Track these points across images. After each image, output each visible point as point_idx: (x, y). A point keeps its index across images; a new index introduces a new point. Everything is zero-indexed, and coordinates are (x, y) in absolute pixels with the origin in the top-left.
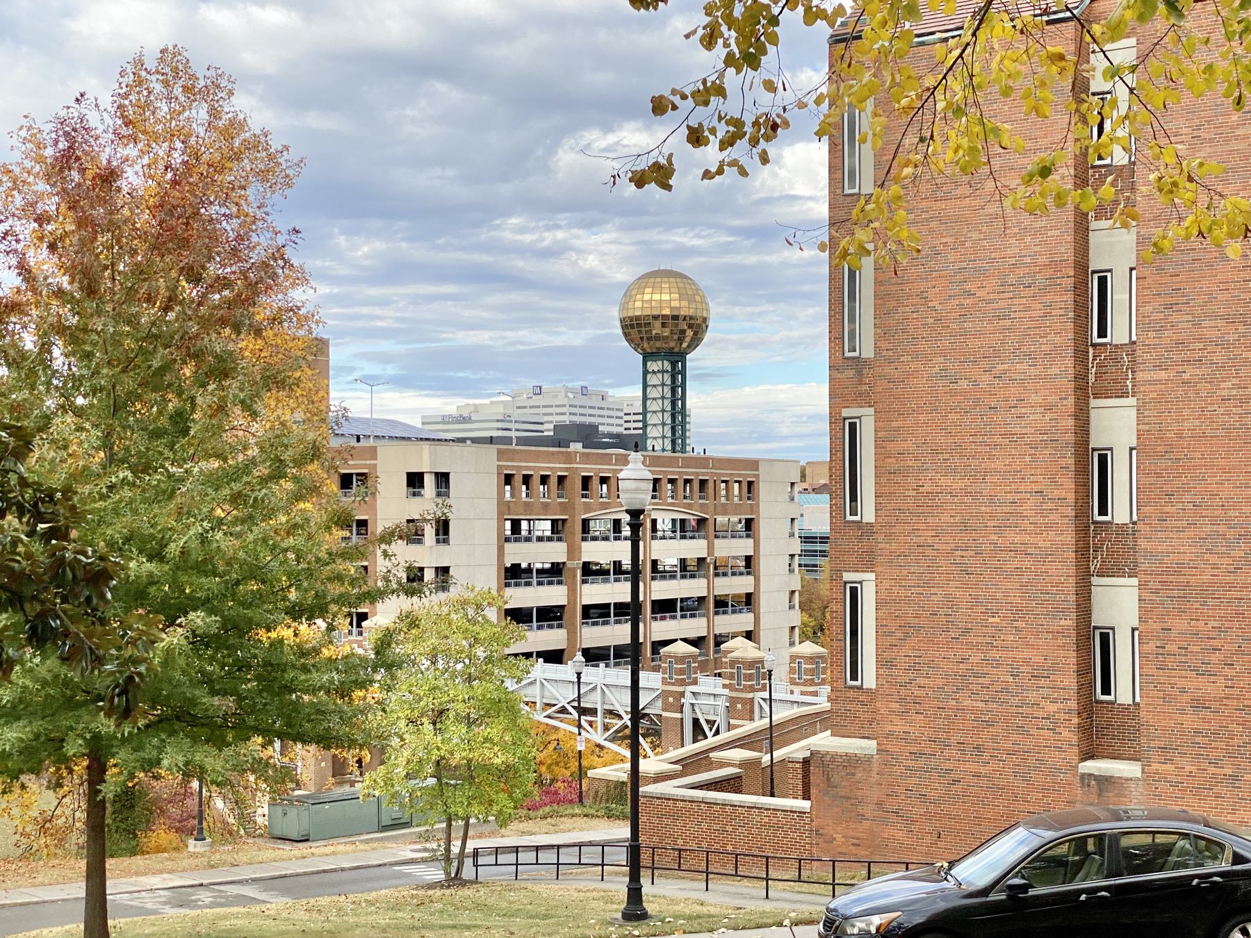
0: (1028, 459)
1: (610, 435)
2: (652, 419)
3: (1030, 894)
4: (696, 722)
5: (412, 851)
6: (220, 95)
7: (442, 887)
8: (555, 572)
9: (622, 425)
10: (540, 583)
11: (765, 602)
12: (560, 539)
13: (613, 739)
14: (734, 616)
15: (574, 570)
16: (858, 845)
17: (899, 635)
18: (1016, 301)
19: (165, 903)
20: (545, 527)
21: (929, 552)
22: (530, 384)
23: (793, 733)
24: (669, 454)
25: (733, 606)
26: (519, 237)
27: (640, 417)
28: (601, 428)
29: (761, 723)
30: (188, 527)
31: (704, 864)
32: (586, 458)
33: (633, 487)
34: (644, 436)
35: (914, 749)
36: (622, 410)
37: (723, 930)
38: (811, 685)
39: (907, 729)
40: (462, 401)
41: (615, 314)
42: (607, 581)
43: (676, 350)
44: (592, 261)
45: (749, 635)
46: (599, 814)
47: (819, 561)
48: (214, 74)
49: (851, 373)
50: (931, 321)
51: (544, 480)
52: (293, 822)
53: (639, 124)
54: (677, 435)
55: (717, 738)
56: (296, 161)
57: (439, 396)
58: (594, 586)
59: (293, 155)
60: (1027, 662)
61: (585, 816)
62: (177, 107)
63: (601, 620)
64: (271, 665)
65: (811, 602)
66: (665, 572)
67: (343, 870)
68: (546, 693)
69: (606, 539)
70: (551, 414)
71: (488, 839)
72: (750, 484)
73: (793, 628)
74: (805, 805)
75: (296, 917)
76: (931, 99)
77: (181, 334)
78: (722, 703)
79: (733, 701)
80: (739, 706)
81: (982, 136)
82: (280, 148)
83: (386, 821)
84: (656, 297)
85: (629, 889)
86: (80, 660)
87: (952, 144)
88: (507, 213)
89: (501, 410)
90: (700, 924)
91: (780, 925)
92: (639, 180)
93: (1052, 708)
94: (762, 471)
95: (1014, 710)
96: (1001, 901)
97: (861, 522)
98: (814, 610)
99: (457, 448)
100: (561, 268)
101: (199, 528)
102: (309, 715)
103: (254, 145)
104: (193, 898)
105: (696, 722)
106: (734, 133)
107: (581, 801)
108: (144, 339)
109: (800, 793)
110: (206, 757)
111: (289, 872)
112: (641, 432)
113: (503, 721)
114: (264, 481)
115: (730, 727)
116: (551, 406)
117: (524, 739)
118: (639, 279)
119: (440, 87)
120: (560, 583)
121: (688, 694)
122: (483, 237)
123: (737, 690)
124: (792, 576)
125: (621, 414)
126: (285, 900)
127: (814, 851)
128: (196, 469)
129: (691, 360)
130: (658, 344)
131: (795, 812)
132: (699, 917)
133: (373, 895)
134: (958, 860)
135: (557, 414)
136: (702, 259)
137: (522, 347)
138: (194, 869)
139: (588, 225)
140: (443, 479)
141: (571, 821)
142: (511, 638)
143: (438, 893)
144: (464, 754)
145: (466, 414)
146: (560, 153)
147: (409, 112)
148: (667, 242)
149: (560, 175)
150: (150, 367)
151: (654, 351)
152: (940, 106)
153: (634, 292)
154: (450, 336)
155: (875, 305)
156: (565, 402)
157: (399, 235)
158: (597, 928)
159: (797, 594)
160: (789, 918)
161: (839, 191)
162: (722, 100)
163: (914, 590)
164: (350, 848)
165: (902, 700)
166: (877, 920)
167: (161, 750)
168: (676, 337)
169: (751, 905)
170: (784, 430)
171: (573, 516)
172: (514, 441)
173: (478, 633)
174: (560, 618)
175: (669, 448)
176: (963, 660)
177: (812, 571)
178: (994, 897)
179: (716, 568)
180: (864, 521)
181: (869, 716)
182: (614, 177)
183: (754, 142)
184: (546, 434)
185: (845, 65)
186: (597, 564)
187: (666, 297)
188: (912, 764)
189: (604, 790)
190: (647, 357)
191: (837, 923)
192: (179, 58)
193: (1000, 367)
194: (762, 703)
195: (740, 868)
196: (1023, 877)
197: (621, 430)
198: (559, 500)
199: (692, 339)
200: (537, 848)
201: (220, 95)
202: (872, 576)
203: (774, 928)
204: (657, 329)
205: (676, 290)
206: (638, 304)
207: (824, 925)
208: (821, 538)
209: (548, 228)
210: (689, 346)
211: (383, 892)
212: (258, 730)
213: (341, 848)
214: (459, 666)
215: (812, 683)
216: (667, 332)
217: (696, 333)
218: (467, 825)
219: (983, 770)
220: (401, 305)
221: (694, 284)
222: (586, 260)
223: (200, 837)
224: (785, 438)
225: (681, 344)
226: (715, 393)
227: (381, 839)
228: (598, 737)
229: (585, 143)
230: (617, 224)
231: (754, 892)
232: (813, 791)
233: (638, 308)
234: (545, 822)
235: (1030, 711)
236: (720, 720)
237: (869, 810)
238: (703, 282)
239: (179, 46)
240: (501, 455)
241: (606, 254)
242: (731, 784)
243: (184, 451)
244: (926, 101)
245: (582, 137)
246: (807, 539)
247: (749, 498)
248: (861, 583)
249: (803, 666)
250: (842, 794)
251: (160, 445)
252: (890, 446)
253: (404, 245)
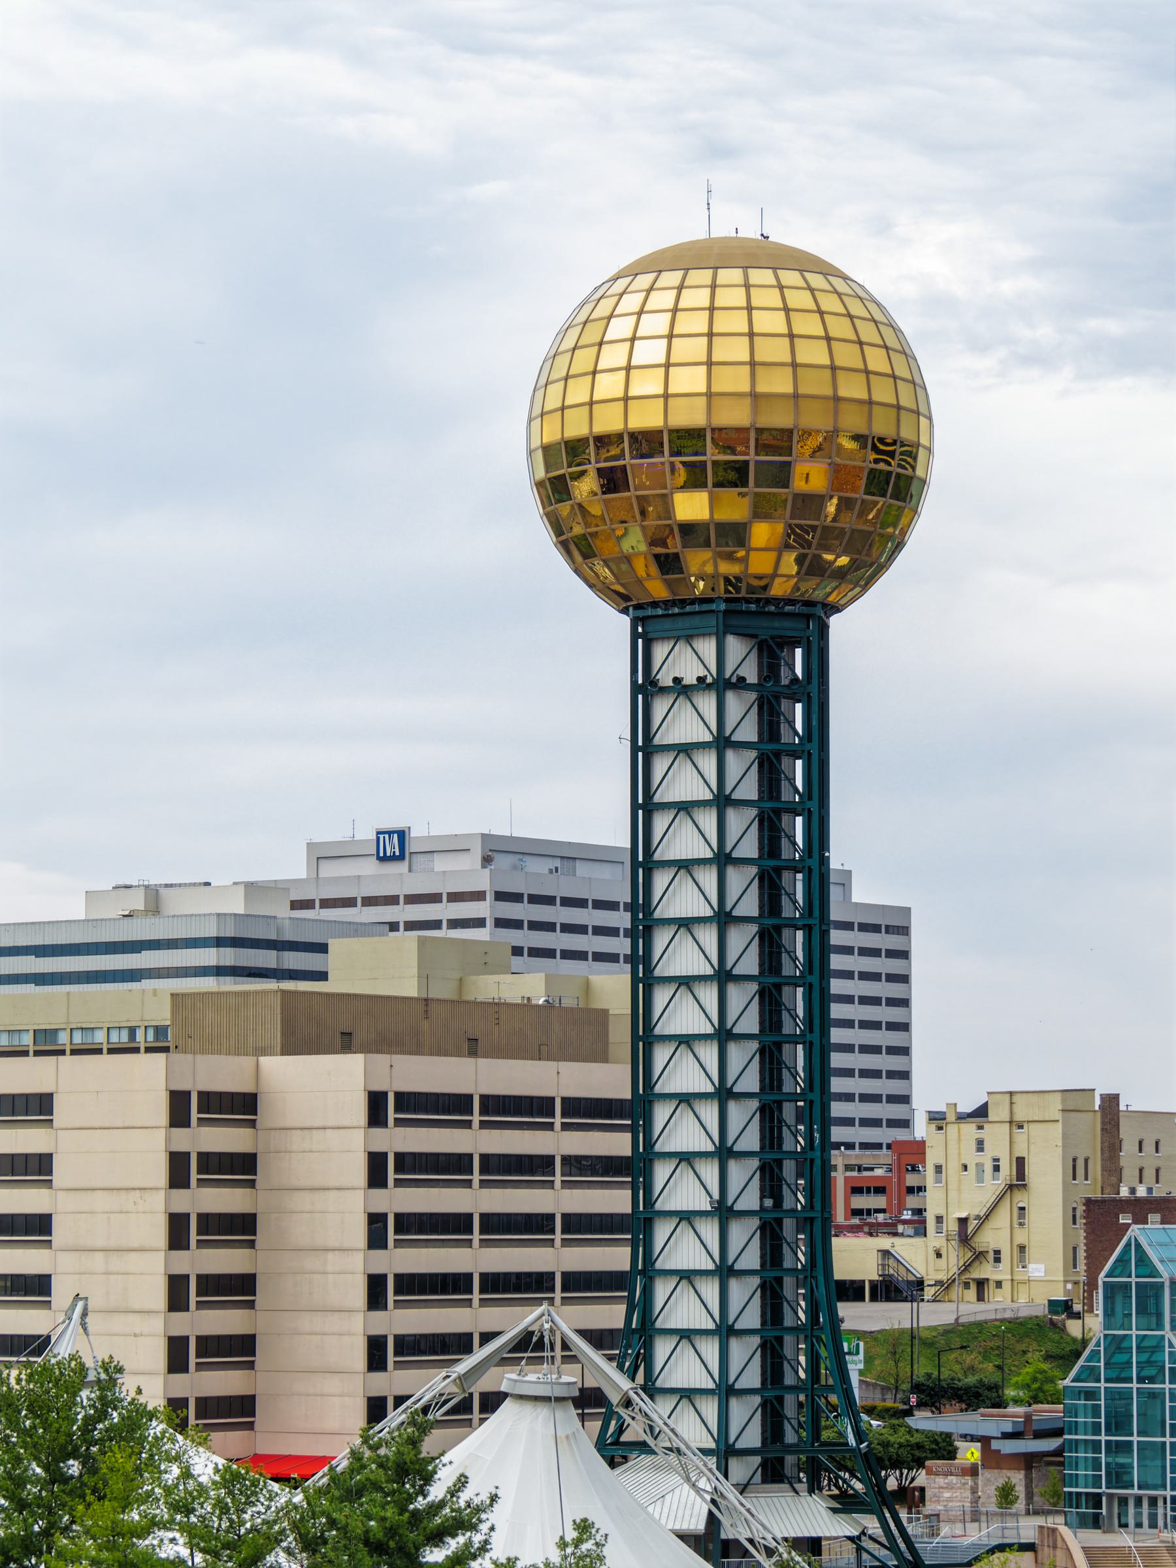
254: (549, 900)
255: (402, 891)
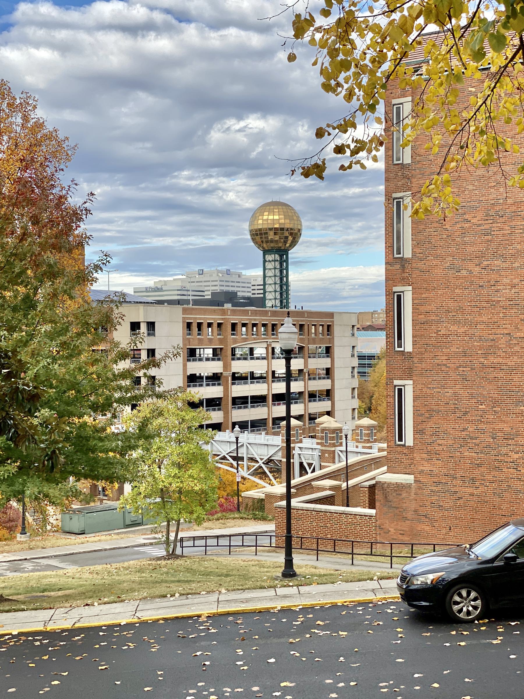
0: (501, 315)
1: (244, 298)
2: (269, 288)
3: (517, 562)
4: (301, 464)
5: (144, 539)
6: (29, 108)
7: (165, 559)
8: (215, 378)
9: (250, 292)
10: (208, 385)
11: (337, 395)
12: (219, 360)
13: (252, 474)
14: (321, 403)
15: (227, 377)
16: (404, 534)
17: (427, 415)
18: (494, 225)
19: (6, 570)
20: (209, 352)
21: (443, 368)
22: (197, 268)
23: (358, 471)
24: (278, 309)
25: (319, 397)
26: (188, 183)
27: (262, 287)
28: (239, 294)
29: (338, 465)
30: (38, 362)
31: (369, 550)
32: (234, 312)
33: (287, 337)
34: (264, 299)
35: (436, 480)
36: (250, 283)
37: (340, 582)
38: (368, 443)
39: (430, 469)
40: (158, 279)
41: (246, 226)
42: (246, 383)
43: (283, 248)
44: (231, 196)
45: (328, 413)
46: (249, 517)
47: (367, 370)
48: (25, 96)
49: (398, 266)
50: (445, 236)
51: (210, 325)
52: (76, 524)
53: (259, 115)
54: (283, 298)
55: (314, 474)
56: (72, 146)
57: (143, 276)
58: (239, 386)
59: (71, 143)
60: (501, 430)
61: (242, 518)
62: (4, 116)
63: (243, 405)
64: (81, 437)
65: (363, 394)
66: (279, 377)
67: (106, 550)
68: (214, 449)
69: (245, 359)
70: (209, 286)
71: (186, 532)
72: (329, 326)
73: (354, 409)
74: (373, 512)
75: (85, 577)
76: (467, 126)
77: (30, 253)
78: (317, 453)
79: (323, 452)
80: (327, 455)
81: (495, 145)
82: (63, 139)
83: (128, 522)
84: (271, 217)
85: (286, 560)
86: (25, 441)
87: (478, 149)
88: (181, 168)
89: (180, 284)
90: (326, 579)
91: (372, 579)
92: (306, 174)
93: (516, 456)
94: (336, 318)
95: (494, 457)
96: (502, 565)
97: (404, 351)
98: (365, 398)
99: (159, 308)
100: (213, 200)
101: (45, 362)
102: (104, 465)
103: (49, 137)
104: (22, 567)
105: (301, 464)
106: (359, 147)
107: (239, 510)
108: (9, 256)
109: (367, 505)
110: (50, 489)
111: (75, 552)
112: (262, 295)
113: (199, 466)
114: (79, 335)
115: (321, 468)
116: (209, 281)
117: (211, 476)
118: (260, 207)
119: (142, 95)
120: (219, 384)
121: (297, 449)
122: (167, 183)
123: (325, 446)
124: (354, 380)
125: (250, 285)
126: (77, 567)
127: (378, 537)
128: (43, 330)
129: (291, 253)
130: (272, 245)
131: (367, 516)
132: (324, 575)
133: (126, 564)
134: (475, 544)
135: (212, 286)
136: (296, 194)
137: (191, 247)
138: (21, 551)
139: (229, 175)
140: (151, 326)
141: (232, 521)
142: (202, 419)
143: (163, 562)
144: (178, 484)
145: (159, 287)
146: (212, 133)
147: (123, 110)
148: (275, 184)
149: (212, 146)
150: (13, 272)
151: (270, 249)
152: (472, 129)
153: (258, 215)
154: (149, 240)
155: (412, 228)
156: (217, 278)
157: (118, 182)
158: (268, 582)
159: (356, 389)
160: (377, 575)
161: (391, 162)
162: (353, 130)
163: (435, 390)
164: (109, 537)
165: (429, 453)
166: (431, 577)
167: (24, 484)
168: (282, 240)
169: (344, 568)
170: (345, 294)
171: (226, 346)
172: (191, 303)
173: (184, 416)
174: (219, 405)
175: (279, 305)
176: (464, 430)
177: (363, 376)
178: (496, 564)
179: (309, 375)
180: (406, 351)
181: (409, 462)
182: (292, 171)
183: (369, 151)
184: (206, 297)
185: (420, 108)
186: (238, 373)
187: (276, 217)
188: (434, 488)
189: (251, 504)
190: (266, 252)
191: (408, 579)
192: (5, 87)
193: (485, 263)
194: (340, 453)
195: (374, 550)
196: (513, 553)
197: (250, 295)
198: (218, 337)
199: (292, 242)
200: (218, 537)
201: (29, 108)
202: (411, 382)
203: (368, 581)
204: (271, 235)
205: (282, 213)
206: (260, 222)
207: (401, 580)
208: (368, 356)
209: (206, 177)
210: (290, 246)
211: (131, 562)
212: (72, 473)
213: (103, 538)
214: (173, 435)
215: (368, 441)
216: (277, 238)
217: (294, 238)
218: (178, 524)
219: (475, 492)
220: (119, 223)
221: (293, 209)
222: (227, 195)
223: (23, 532)
224: (345, 298)
225: (285, 245)
226: (304, 272)
227: (125, 533)
228: (244, 473)
229: (227, 127)
230: (246, 174)
231: (344, 561)
232: (377, 504)
233: (260, 223)
234: (218, 522)
235: (503, 458)
236: (316, 463)
237: (410, 515)
238: (297, 208)
239: (5, 80)
240: (185, 311)
241: (239, 192)
242: (328, 500)
243: (33, 320)
244: (464, 127)
245: (225, 123)
246: (361, 357)
247: (328, 335)
248: (404, 386)
249: (364, 432)
250: (394, 505)
251: (19, 315)
252: (422, 309)
253: (121, 188)
254: (228, 281)
255: (203, 280)
